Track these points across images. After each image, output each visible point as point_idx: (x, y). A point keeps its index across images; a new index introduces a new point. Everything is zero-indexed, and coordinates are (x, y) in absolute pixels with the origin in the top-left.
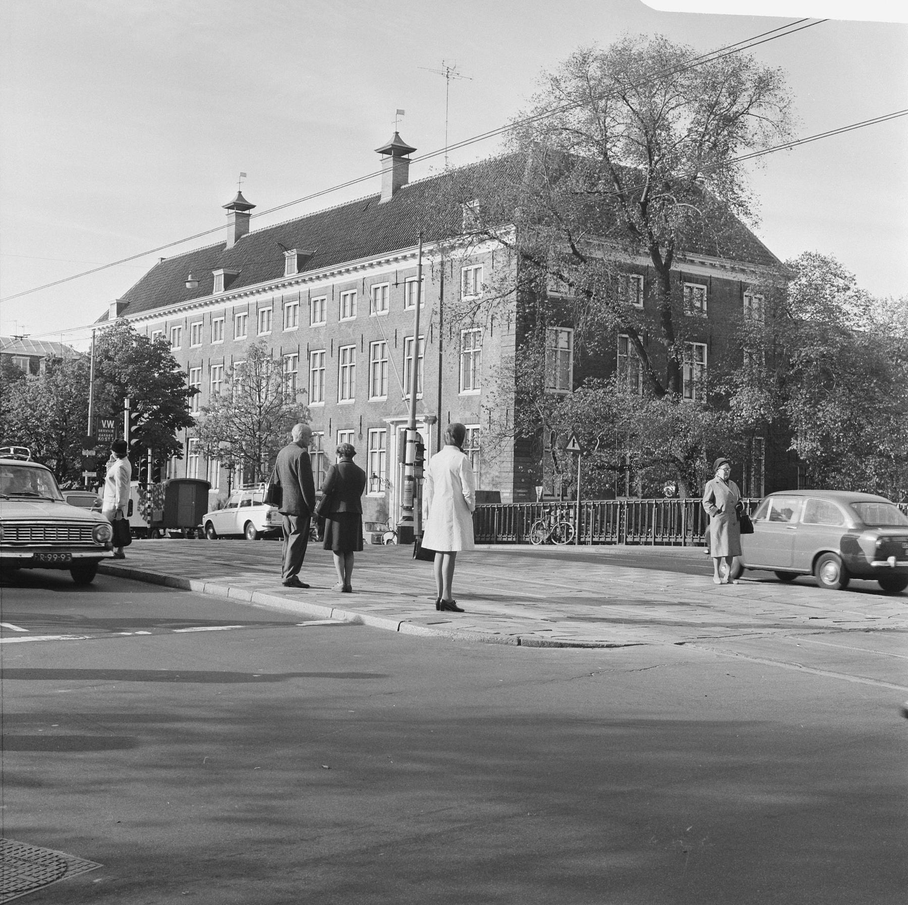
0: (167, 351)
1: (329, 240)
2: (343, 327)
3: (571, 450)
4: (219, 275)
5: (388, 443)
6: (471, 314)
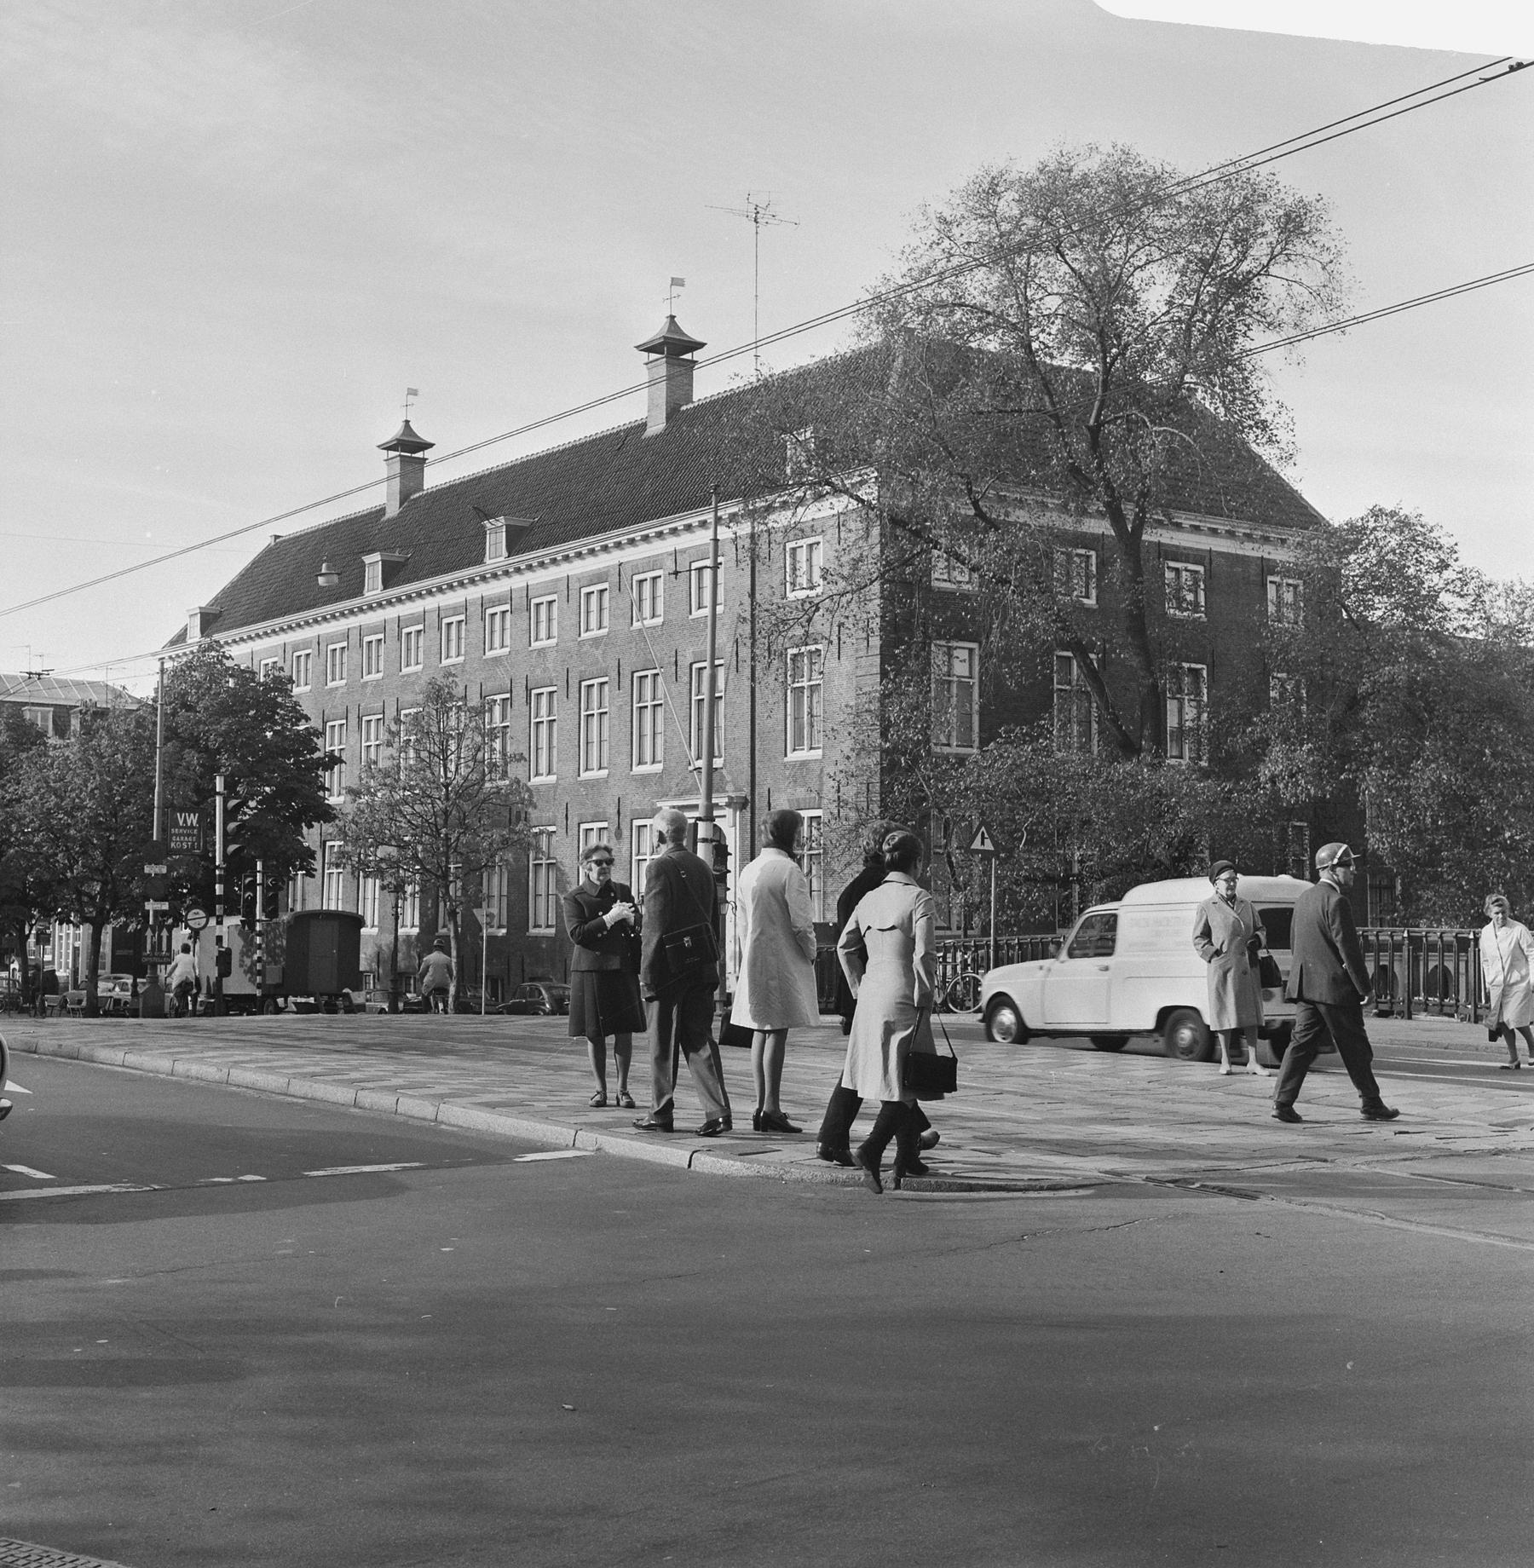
0: (287, 693)
3: (978, 851)
4: (373, 561)
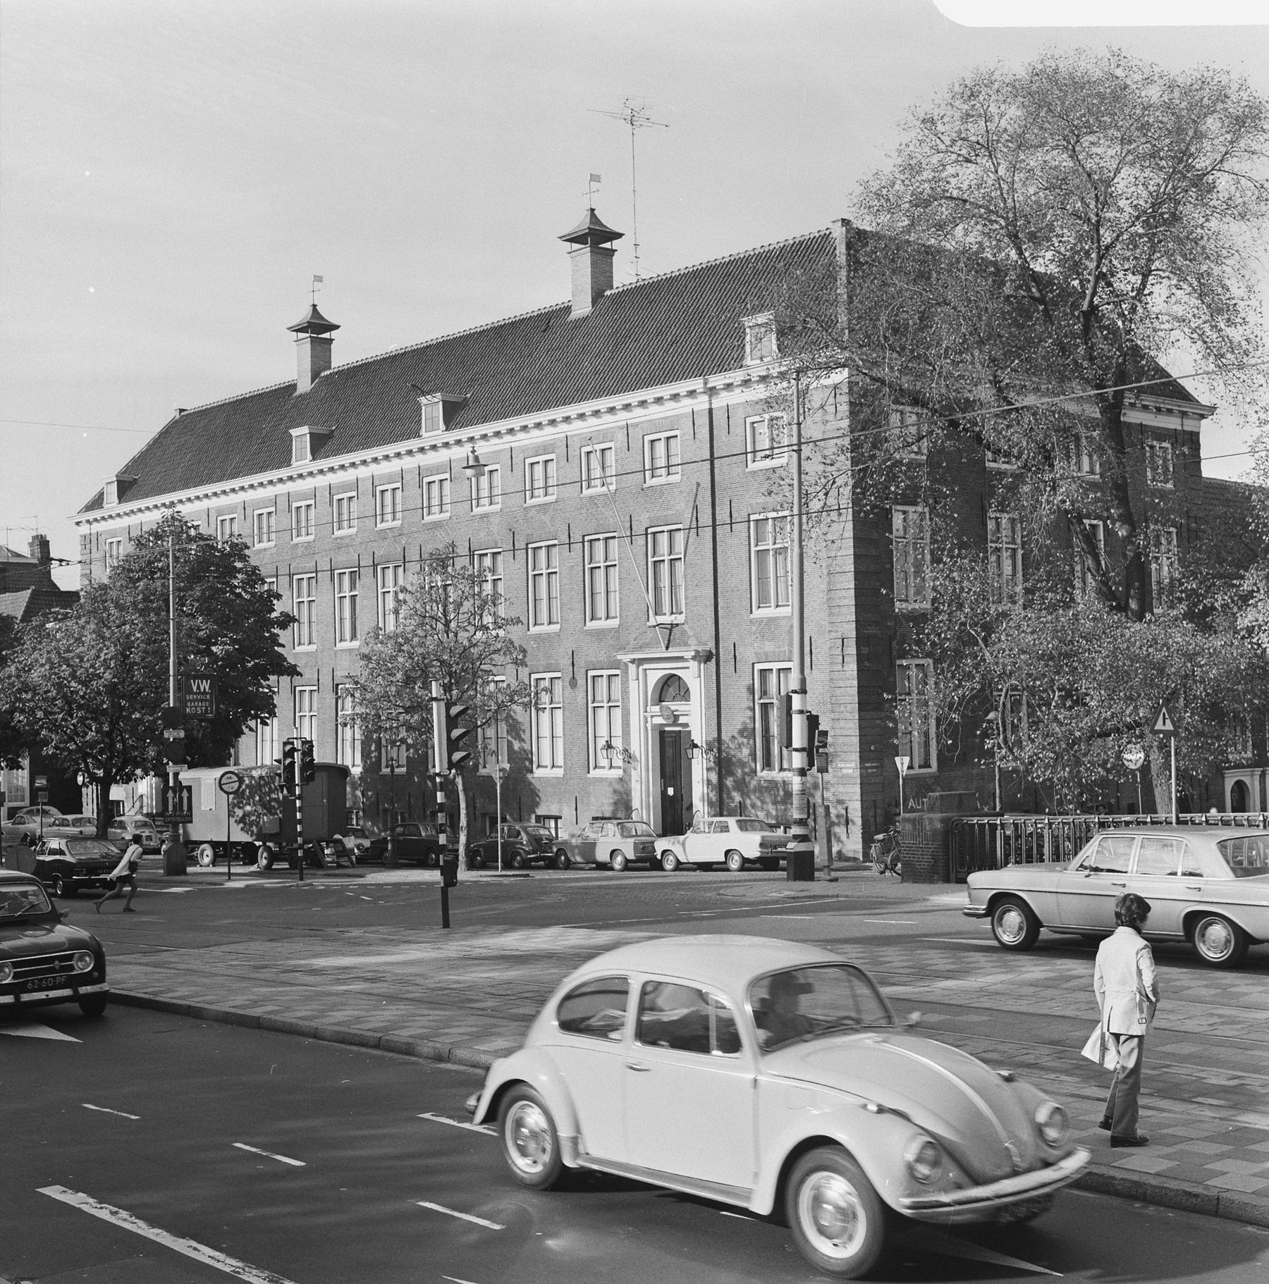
0: (244, 558)
1: (489, 370)
2: (533, 512)
3: (1161, 732)
4: (301, 434)
5: (625, 692)
6: (821, 495)
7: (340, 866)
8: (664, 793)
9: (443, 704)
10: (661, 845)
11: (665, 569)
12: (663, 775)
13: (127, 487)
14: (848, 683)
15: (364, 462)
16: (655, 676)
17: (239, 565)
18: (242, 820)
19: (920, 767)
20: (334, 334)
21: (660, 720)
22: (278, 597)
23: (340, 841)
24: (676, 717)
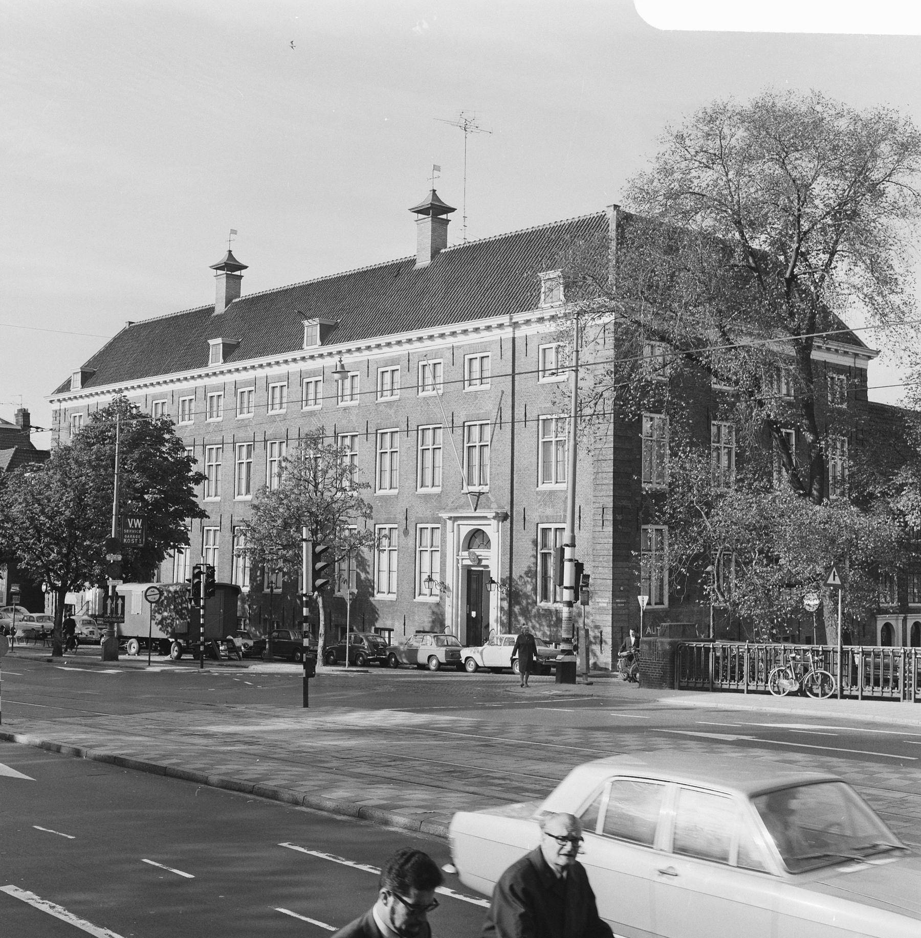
0: (170, 432)
1: (357, 303)
4: (216, 343)
5: (444, 541)
7: (230, 659)
8: (469, 615)
9: (310, 544)
10: (465, 653)
11: (476, 452)
12: (469, 602)
13: (88, 376)
14: (606, 541)
15: (261, 366)
16: (465, 530)
17: (167, 436)
18: (161, 623)
19: (656, 604)
20: (243, 272)
21: (468, 562)
22: (195, 461)
23: (231, 641)
24: (480, 560)
